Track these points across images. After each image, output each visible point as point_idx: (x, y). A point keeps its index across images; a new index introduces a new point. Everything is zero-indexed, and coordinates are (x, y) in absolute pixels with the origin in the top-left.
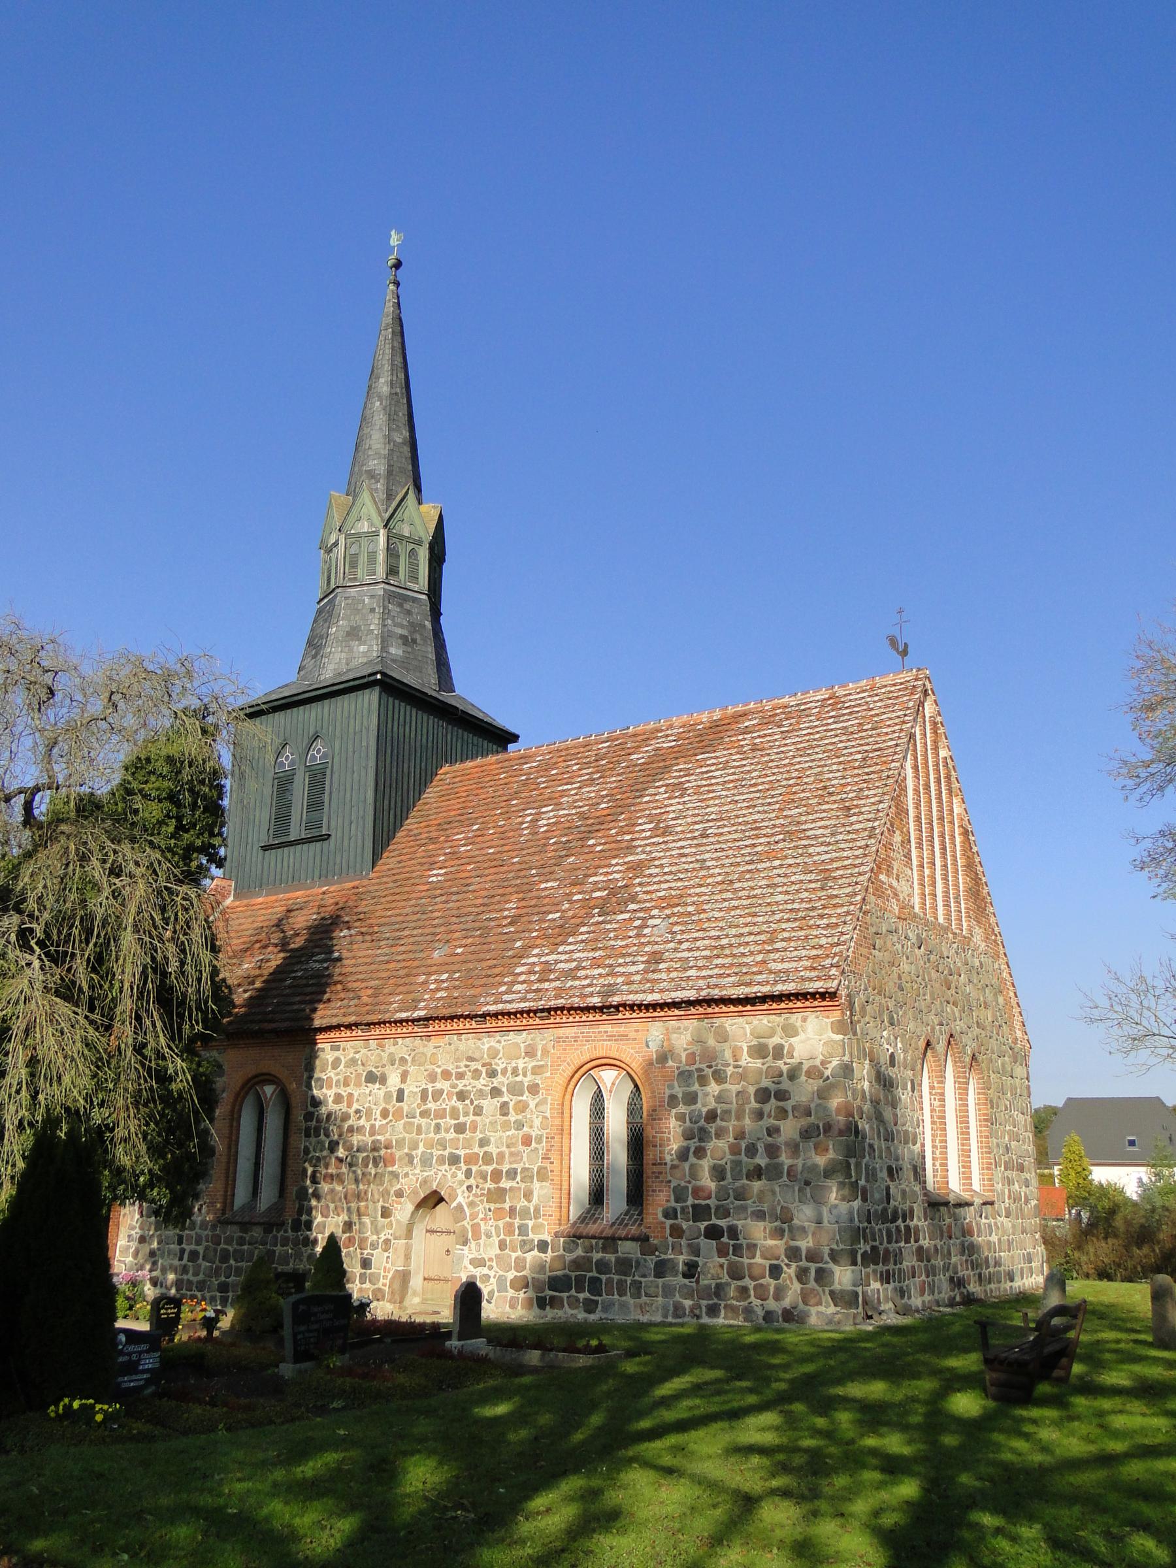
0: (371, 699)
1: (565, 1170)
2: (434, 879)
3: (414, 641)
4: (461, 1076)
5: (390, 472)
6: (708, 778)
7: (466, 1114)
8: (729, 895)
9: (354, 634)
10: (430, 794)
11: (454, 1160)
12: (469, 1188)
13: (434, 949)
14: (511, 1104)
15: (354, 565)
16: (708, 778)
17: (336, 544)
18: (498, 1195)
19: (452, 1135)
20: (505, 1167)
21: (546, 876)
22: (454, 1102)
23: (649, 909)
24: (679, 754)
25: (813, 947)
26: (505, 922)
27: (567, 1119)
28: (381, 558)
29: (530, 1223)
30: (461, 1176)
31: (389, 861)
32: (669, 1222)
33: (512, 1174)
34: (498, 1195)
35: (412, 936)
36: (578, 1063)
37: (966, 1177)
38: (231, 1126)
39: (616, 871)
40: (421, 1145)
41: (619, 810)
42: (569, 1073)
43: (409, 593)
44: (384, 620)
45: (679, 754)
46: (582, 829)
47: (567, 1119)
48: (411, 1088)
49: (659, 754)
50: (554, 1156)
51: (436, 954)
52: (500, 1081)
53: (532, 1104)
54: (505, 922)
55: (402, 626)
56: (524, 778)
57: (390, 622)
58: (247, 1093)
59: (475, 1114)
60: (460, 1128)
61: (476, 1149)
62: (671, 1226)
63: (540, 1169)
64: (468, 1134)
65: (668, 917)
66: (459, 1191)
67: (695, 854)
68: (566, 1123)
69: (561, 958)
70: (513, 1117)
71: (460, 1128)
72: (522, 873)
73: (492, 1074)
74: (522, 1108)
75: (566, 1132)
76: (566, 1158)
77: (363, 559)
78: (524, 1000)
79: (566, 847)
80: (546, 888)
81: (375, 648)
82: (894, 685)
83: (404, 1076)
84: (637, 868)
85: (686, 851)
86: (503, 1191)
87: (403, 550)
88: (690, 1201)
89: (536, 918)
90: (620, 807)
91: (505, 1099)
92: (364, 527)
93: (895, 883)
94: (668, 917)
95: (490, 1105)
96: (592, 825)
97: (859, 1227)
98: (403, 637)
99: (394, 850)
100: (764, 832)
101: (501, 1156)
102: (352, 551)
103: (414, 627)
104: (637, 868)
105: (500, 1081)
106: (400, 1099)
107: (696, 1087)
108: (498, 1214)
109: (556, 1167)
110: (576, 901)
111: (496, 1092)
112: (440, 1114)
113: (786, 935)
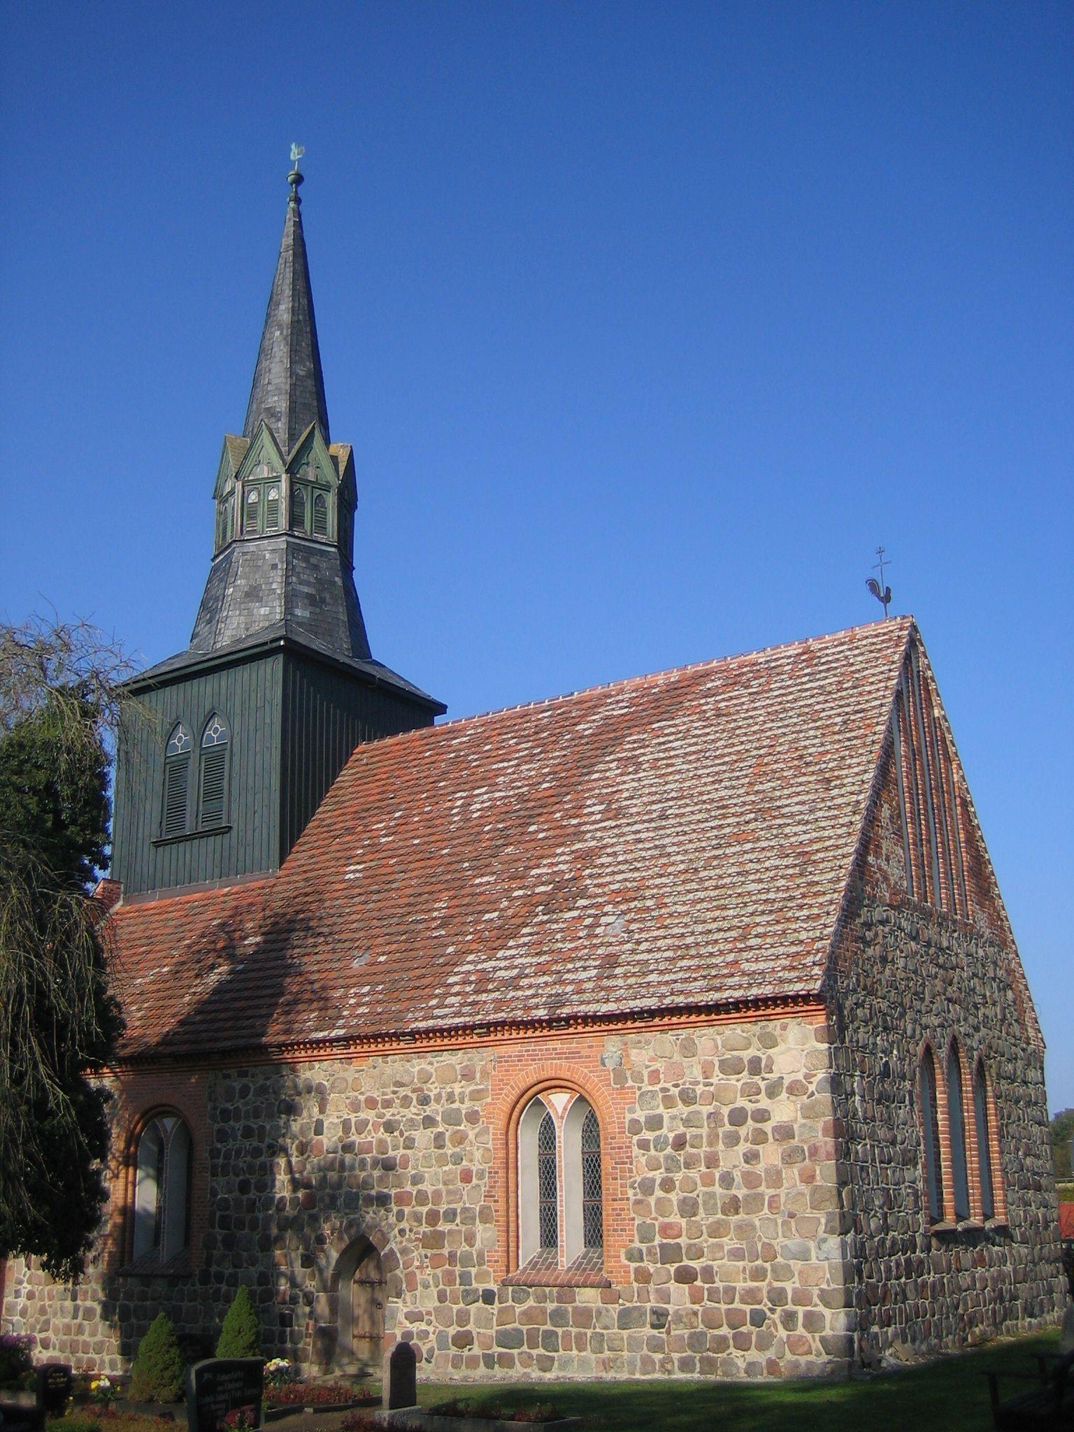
4: (388, 1104)
5: (292, 410)
9: (253, 594)
10: (345, 776)
14: (447, 1134)
20: (443, 1208)
22: (381, 1134)
32: (633, 1265)
34: (435, 1240)
39: (562, 862)
50: (499, 1193)
52: (433, 1109)
53: (471, 1135)
56: (452, 755)
63: (483, 1209)
70: (449, 1150)
74: (460, 1139)
81: (278, 610)
84: (586, 857)
88: (658, 1240)
89: (470, 919)
91: (440, 1129)
95: (423, 1137)
101: (437, 1194)
104: (586, 857)
105: (433, 1109)
108: (436, 1262)
109: (501, 1205)
110: (515, 898)
111: (429, 1122)
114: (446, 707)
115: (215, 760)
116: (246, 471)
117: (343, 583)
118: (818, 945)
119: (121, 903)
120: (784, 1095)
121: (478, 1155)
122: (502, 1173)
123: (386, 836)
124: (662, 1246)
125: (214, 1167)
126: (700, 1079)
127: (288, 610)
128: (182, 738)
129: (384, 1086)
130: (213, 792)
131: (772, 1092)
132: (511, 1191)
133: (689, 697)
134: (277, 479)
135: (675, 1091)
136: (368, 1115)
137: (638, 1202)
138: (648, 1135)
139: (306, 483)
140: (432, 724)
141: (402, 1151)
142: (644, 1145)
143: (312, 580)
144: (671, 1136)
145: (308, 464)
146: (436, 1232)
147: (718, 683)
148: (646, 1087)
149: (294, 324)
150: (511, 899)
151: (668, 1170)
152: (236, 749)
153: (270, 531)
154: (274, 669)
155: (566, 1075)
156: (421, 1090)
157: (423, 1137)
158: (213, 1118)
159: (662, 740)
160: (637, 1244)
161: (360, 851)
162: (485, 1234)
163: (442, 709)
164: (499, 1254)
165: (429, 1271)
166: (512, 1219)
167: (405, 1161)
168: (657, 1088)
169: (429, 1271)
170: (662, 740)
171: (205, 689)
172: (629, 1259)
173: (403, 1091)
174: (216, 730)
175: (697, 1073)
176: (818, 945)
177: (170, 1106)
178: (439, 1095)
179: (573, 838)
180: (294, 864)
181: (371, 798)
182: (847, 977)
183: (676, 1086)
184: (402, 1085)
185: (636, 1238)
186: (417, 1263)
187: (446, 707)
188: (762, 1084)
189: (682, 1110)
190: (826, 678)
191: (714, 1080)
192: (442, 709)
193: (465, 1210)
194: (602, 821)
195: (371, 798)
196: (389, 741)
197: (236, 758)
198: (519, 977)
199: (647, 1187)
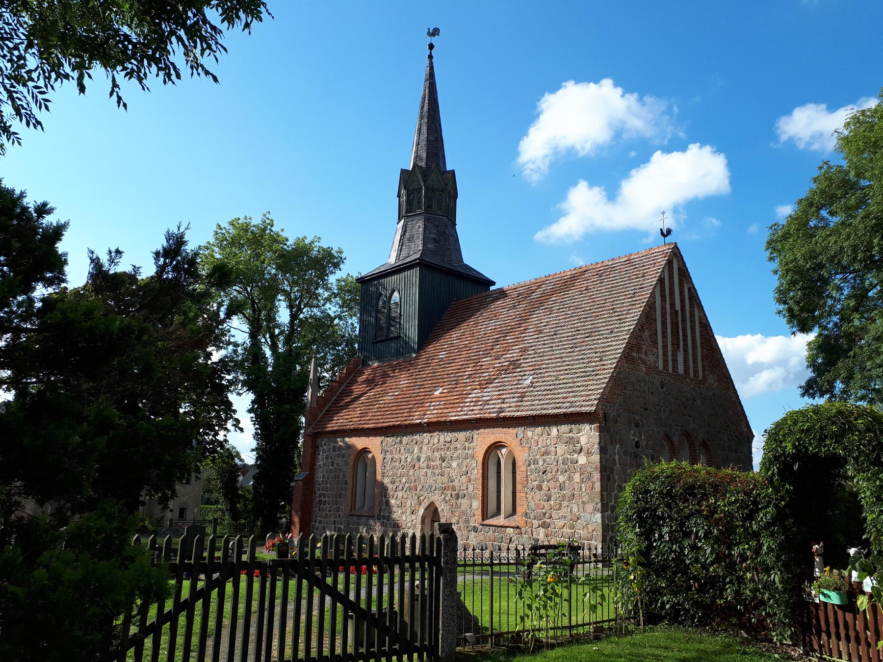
2: (441, 357)
3: (440, 241)
6: (563, 305)
13: (436, 390)
16: (563, 305)
21: (486, 355)
24: (554, 292)
25: (589, 390)
26: (465, 377)
37: (387, 554)
38: (354, 472)
43: (439, 217)
45: (554, 292)
49: (543, 294)
54: (465, 377)
55: (434, 234)
57: (427, 232)
69: (490, 392)
78: (466, 414)
80: (484, 361)
82: (643, 256)
84: (524, 350)
85: (546, 342)
93: (644, 357)
97: (608, 525)
98: (434, 239)
100: (581, 332)
106: (419, 460)
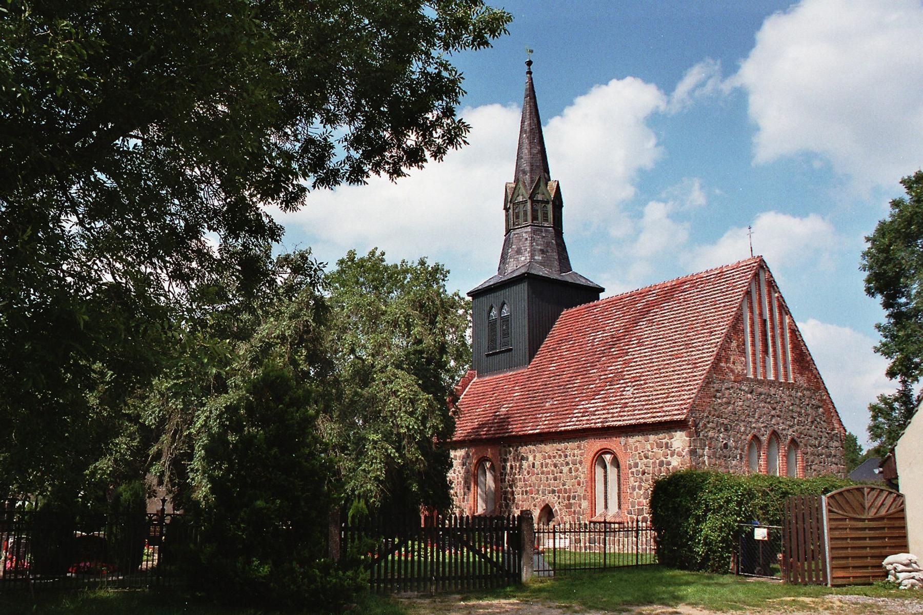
0: (523, 288)
1: (593, 495)
4: (554, 457)
5: (532, 170)
7: (557, 473)
8: (658, 376)
9: (519, 252)
10: (557, 324)
11: (554, 491)
12: (559, 503)
14: (573, 469)
15: (517, 217)
17: (509, 208)
18: (569, 506)
19: (552, 481)
20: (572, 494)
22: (553, 468)
23: (627, 383)
27: (593, 474)
28: (529, 213)
29: (581, 517)
30: (556, 498)
31: (536, 360)
32: (629, 516)
33: (574, 498)
34: (569, 506)
35: (540, 396)
36: (595, 451)
39: (618, 365)
40: (542, 486)
41: (626, 333)
42: (593, 455)
44: (532, 243)
46: (611, 343)
47: (593, 474)
48: (537, 463)
50: (589, 489)
51: (547, 404)
52: (569, 459)
53: (580, 468)
56: (593, 316)
58: (479, 465)
59: (561, 473)
60: (555, 479)
61: (561, 487)
62: (630, 517)
63: (584, 495)
64: (558, 481)
65: (634, 386)
66: (556, 505)
67: (650, 355)
68: (593, 476)
70: (573, 474)
71: (555, 479)
72: (585, 365)
73: (566, 456)
74: (577, 470)
75: (593, 480)
76: (593, 490)
77: (522, 214)
79: (603, 352)
81: (528, 258)
83: (535, 457)
84: (626, 363)
86: (571, 504)
87: (539, 207)
88: (637, 507)
89: (586, 387)
90: (627, 331)
91: (571, 466)
92: (520, 199)
93: (731, 365)
94: (634, 386)
95: (565, 469)
96: (616, 340)
99: (539, 354)
101: (570, 489)
102: (517, 211)
103: (548, 244)
104: (626, 363)
105: (569, 459)
106: (533, 467)
107: (638, 461)
108: (570, 513)
109: (589, 494)
110: (602, 379)
111: (567, 464)
112: (548, 473)
113: (673, 394)
114: (604, 289)
115: (506, 320)
116: (514, 199)
117: (556, 242)
118: (688, 401)
119: (476, 378)
120: (675, 456)
121: (582, 476)
122: (590, 483)
123: (566, 351)
124: (638, 509)
125: (501, 479)
126: (650, 449)
127: (532, 256)
128: (494, 313)
129: (554, 451)
130: (506, 334)
131: (672, 455)
132: (593, 489)
133: (677, 292)
134: (526, 202)
135: (642, 454)
136: (548, 461)
137: (631, 493)
138: (634, 470)
139: (538, 201)
140: (598, 299)
141: (559, 474)
142: (632, 473)
143: (542, 243)
144: (641, 470)
145: (538, 193)
146: (570, 503)
147: (688, 286)
148: (634, 453)
149: (531, 130)
150: (600, 380)
151: (640, 482)
152: (512, 318)
153: (524, 224)
154: (523, 288)
155: (609, 447)
156: (565, 452)
157: (565, 469)
158: (501, 462)
159: (663, 312)
160: (630, 508)
161: (556, 358)
162: (585, 504)
163: (603, 290)
164: (589, 511)
165: (568, 517)
166: (593, 498)
167: (560, 477)
168: (637, 453)
169: (568, 517)
170: (663, 312)
171: (501, 295)
172: (628, 514)
173: (559, 452)
174: (506, 310)
175: (649, 447)
176: (688, 401)
177: (606, 449)
178: (570, 454)
179: (625, 354)
180: (535, 363)
181: (563, 335)
182: (703, 412)
183: (643, 452)
184: (559, 450)
185: (630, 506)
186: (564, 514)
187: (604, 289)
188: (669, 452)
189: (645, 460)
190: (724, 285)
191: (654, 450)
192: (603, 290)
193: (578, 495)
194: (636, 347)
195: (563, 335)
196: (574, 309)
197: (513, 321)
198: (596, 411)
199: (634, 489)
